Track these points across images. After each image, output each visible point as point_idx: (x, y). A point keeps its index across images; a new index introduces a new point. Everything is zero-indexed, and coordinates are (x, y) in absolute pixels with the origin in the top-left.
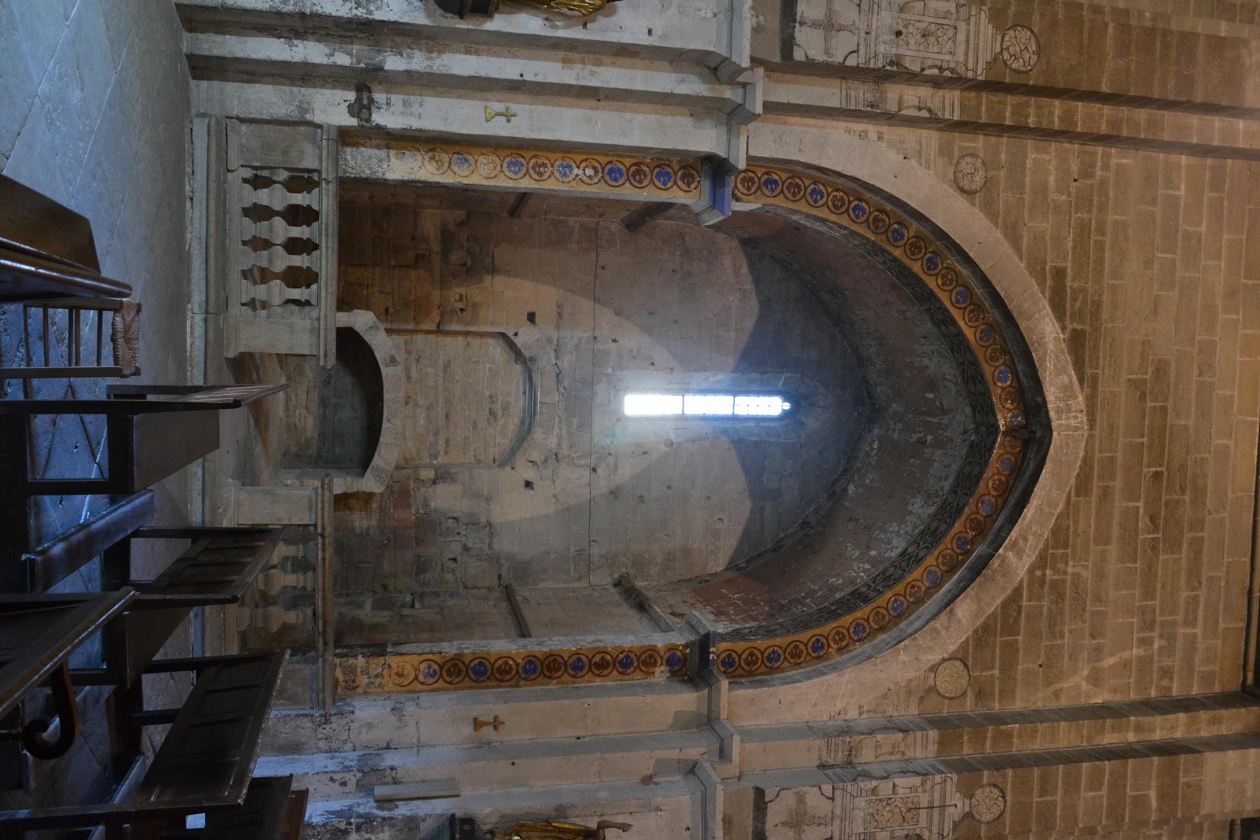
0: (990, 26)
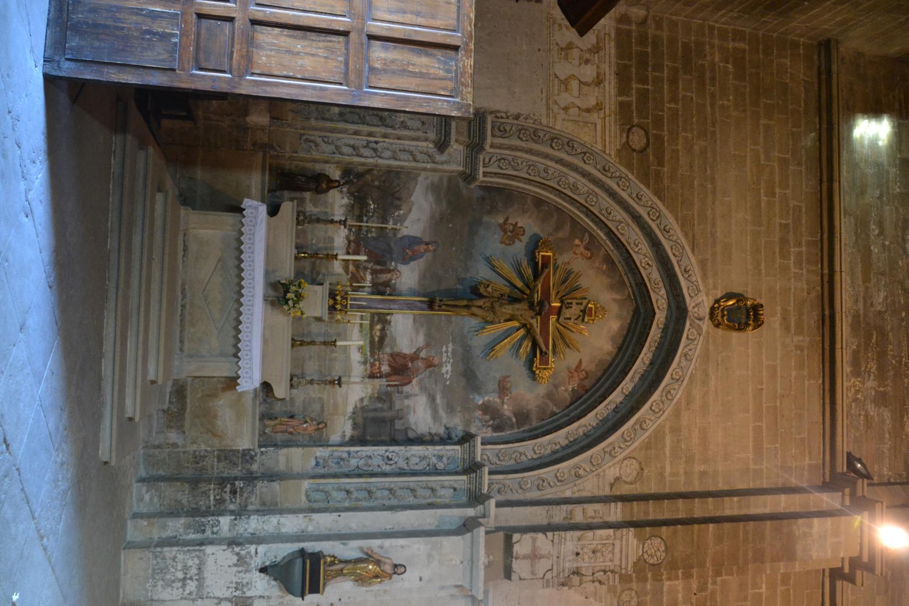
0: (635, 540)
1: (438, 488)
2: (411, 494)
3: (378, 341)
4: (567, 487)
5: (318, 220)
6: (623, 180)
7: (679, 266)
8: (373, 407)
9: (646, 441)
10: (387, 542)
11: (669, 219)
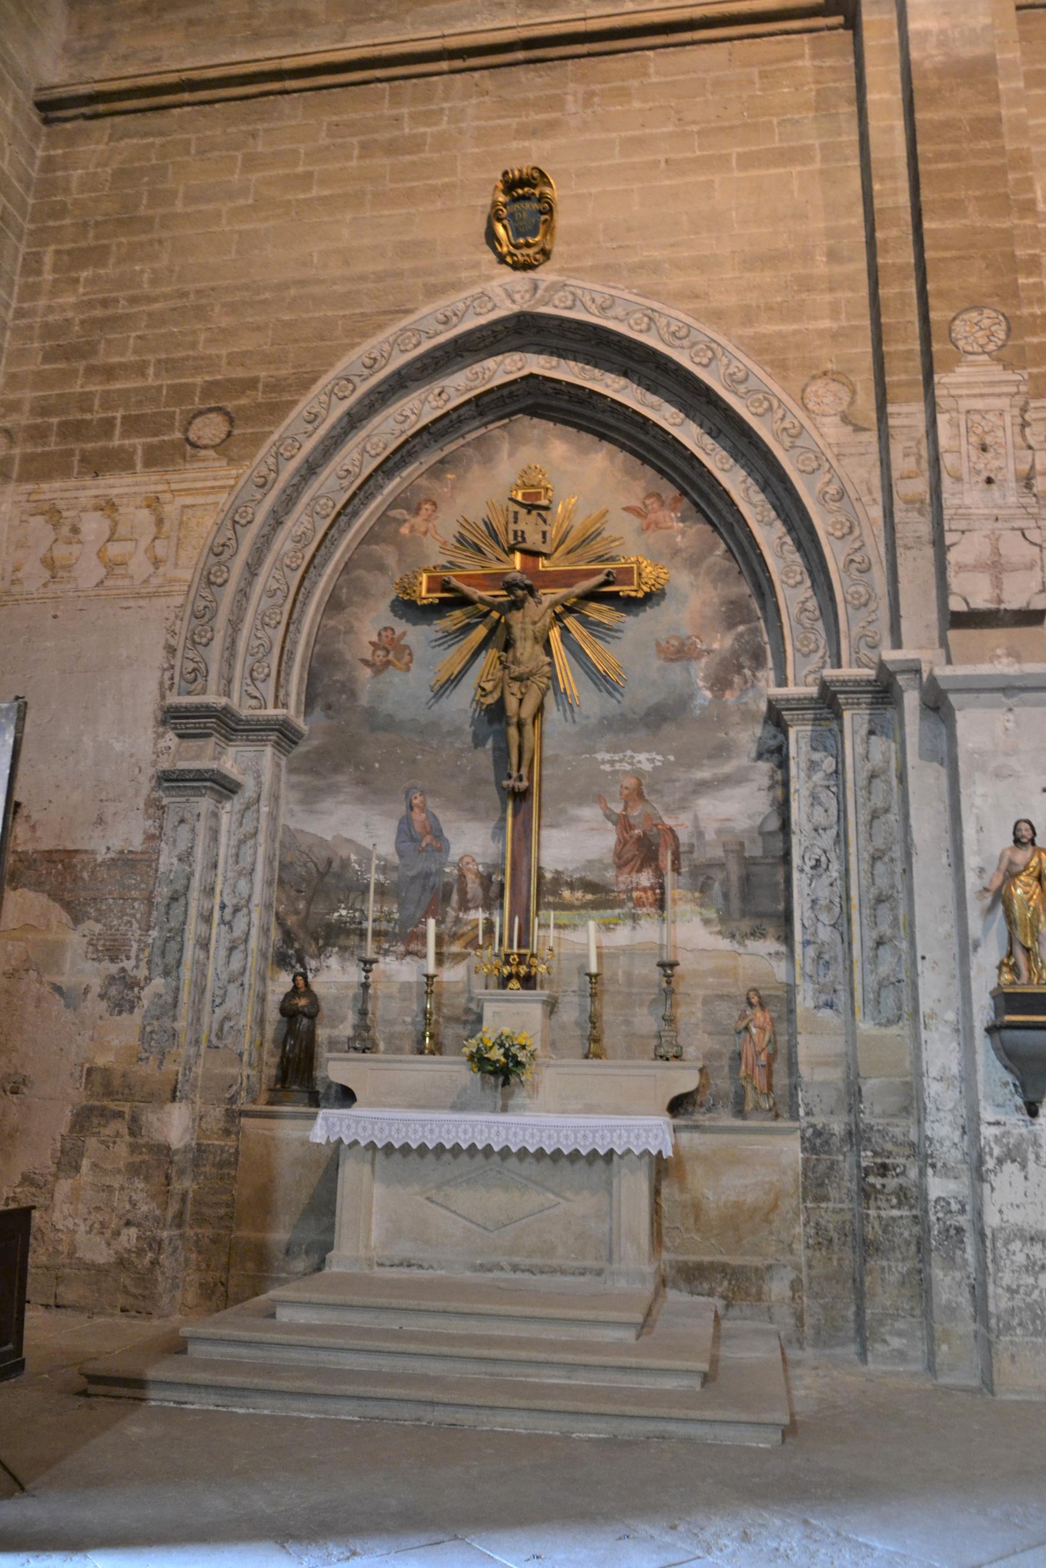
0: (958, 370)
1: (869, 766)
2: (883, 819)
3: (593, 894)
4: (862, 516)
5: (363, 1013)
6: (281, 450)
7: (437, 334)
8: (720, 900)
9: (769, 370)
10: (971, 861)
11: (351, 360)
